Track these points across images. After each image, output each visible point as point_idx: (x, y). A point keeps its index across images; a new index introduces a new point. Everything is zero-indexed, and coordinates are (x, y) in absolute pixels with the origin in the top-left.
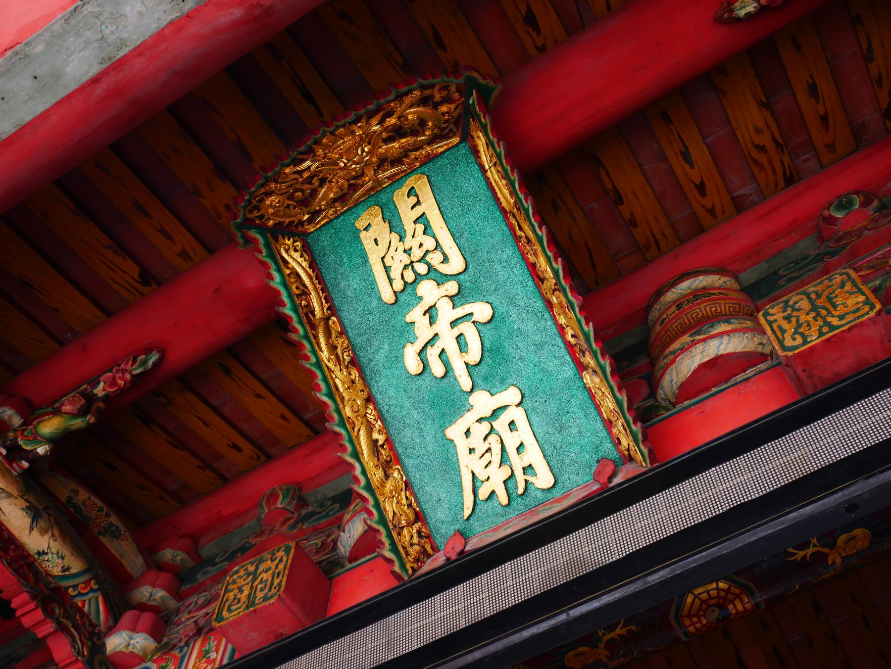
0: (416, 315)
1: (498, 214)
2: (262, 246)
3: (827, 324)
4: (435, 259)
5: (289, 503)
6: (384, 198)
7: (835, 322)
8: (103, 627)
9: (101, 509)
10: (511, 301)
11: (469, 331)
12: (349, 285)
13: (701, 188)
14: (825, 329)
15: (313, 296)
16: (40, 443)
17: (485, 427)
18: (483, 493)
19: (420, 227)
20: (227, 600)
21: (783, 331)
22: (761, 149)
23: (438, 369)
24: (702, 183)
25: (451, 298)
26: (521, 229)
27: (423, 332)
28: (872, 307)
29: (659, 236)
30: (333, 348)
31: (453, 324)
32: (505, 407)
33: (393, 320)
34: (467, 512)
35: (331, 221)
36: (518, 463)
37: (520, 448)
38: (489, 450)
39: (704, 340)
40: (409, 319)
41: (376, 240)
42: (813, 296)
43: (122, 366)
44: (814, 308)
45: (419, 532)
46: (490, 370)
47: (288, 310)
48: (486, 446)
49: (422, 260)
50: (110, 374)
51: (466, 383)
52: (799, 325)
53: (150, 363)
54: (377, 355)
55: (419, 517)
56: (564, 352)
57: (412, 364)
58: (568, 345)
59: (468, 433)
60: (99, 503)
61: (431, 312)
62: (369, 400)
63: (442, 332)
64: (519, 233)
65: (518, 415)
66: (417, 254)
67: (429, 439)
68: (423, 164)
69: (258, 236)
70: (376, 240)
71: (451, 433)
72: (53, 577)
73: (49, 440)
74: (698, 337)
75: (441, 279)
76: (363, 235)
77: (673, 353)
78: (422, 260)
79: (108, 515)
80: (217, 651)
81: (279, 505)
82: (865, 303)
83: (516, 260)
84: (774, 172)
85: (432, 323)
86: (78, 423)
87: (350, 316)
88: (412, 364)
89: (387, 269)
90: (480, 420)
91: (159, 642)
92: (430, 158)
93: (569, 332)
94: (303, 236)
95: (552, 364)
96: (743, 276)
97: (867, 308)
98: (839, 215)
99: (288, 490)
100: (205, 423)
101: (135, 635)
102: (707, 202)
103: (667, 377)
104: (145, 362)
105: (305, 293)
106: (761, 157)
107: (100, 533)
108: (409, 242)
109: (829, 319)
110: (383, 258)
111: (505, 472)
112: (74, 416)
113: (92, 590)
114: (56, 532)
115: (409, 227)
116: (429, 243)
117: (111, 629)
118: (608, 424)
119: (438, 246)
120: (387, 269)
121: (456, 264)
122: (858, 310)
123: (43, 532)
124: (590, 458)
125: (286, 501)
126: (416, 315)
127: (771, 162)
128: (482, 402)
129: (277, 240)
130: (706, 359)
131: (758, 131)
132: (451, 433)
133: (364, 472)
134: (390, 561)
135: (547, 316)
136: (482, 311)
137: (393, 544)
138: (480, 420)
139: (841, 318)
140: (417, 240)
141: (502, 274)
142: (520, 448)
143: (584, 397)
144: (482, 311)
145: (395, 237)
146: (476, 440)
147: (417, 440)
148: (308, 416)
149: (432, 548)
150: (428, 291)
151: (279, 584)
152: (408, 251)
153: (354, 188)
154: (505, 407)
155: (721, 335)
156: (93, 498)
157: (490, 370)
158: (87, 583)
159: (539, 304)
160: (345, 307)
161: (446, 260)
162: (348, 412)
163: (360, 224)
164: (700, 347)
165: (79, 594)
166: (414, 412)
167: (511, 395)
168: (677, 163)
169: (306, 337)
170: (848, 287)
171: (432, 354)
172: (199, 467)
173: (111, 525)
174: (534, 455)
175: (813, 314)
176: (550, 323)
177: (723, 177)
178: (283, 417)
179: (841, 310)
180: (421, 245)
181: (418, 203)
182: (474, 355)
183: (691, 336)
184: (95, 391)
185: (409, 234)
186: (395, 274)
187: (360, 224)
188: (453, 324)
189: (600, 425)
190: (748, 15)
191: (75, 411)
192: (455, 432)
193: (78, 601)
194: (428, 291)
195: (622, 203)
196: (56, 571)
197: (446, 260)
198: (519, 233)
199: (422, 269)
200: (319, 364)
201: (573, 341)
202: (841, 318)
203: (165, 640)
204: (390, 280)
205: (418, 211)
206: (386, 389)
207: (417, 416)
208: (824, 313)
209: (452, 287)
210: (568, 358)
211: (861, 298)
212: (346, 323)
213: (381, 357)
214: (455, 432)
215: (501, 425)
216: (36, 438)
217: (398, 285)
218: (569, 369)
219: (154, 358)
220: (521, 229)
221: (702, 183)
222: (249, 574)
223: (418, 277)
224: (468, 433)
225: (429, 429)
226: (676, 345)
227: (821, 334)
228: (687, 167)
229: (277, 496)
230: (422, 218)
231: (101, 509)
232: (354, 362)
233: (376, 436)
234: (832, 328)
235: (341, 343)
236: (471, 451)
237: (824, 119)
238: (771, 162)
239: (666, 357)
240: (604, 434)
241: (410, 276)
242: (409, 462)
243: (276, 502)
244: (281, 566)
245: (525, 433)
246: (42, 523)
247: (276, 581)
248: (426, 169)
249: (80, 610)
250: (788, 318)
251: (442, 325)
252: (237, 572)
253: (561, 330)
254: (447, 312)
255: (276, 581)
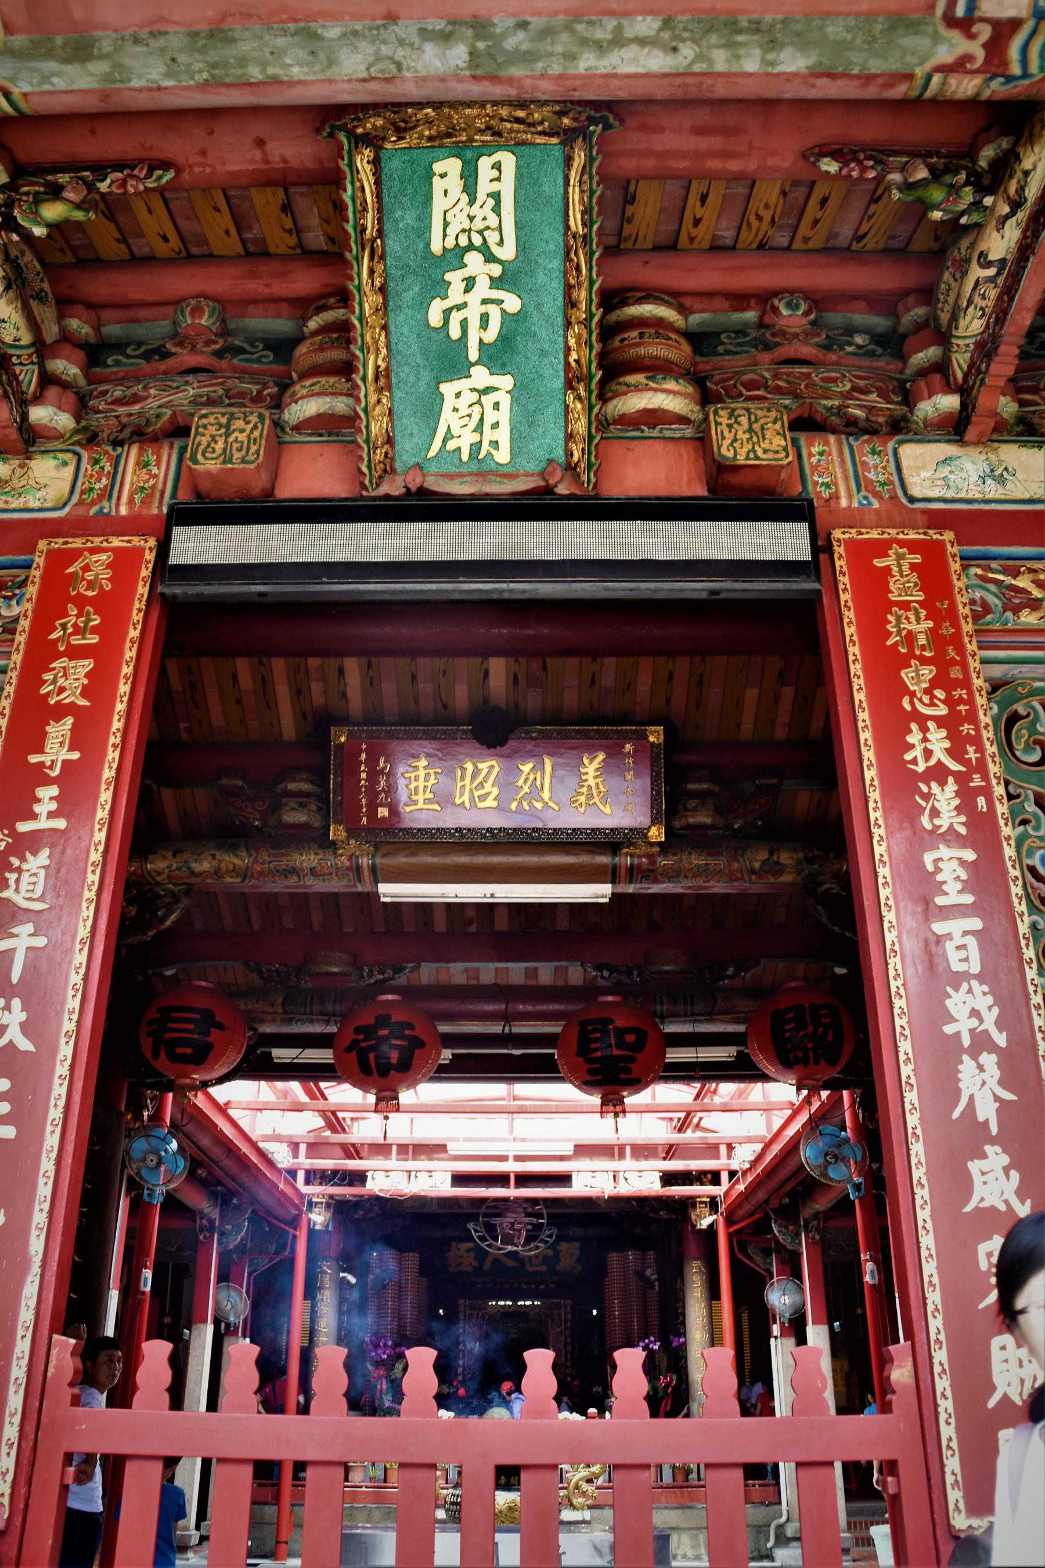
0: (455, 278)
1: (561, 227)
2: (345, 153)
3: (755, 452)
4: (492, 237)
5: (214, 323)
6: (469, 154)
7: (760, 453)
8: (29, 397)
9: (38, 274)
10: (538, 306)
11: (494, 311)
12: (405, 217)
13: (697, 222)
14: (751, 455)
15: (370, 216)
16: (39, 224)
17: (475, 396)
18: (451, 445)
19: (491, 202)
20: (199, 444)
21: (723, 438)
22: (760, 218)
23: (455, 332)
24: (700, 219)
25: (491, 278)
26: (576, 253)
27: (456, 294)
28: (787, 456)
29: (641, 236)
30: (372, 272)
31: (484, 302)
32: (497, 389)
33: (434, 271)
34: (431, 454)
35: (410, 148)
36: (488, 435)
37: (495, 426)
38: (470, 416)
39: (656, 390)
40: (448, 277)
41: (446, 192)
42: (753, 417)
43: (136, 172)
44: (750, 430)
45: (386, 454)
46: (496, 355)
47: (349, 228)
48: (469, 411)
49: (481, 232)
50: (120, 175)
51: (473, 355)
52: (735, 440)
53: (164, 180)
54: (408, 292)
55: (390, 441)
56: (561, 367)
57: (435, 318)
58: (567, 364)
59: (458, 395)
60: (38, 267)
61: (470, 283)
62: (384, 327)
63: (472, 305)
64: (573, 256)
65: (505, 400)
66: (478, 224)
67: (423, 383)
68: (517, 144)
69: (345, 141)
70: (446, 192)
71: (444, 388)
72: (4, 343)
73: (49, 225)
74: (654, 385)
75: (490, 258)
76: (436, 180)
77: (627, 385)
78: (481, 232)
79: (42, 281)
80: (158, 465)
81: (203, 322)
82: (785, 449)
83: (559, 275)
84: (756, 236)
85: (467, 290)
86: (79, 215)
87: (393, 244)
88: (435, 318)
89: (446, 224)
90: (472, 390)
91: (78, 422)
92: (524, 143)
93: (574, 356)
94: (378, 149)
95: (548, 373)
96: (695, 319)
97: (783, 454)
98: (785, 312)
99: (214, 309)
100: (150, 211)
101: (60, 413)
102: (694, 232)
103: (614, 402)
104: (160, 178)
105: (365, 210)
106: (755, 223)
107: (31, 296)
108: (475, 210)
109: (757, 448)
110: (445, 212)
111: (476, 438)
112: (78, 206)
113: (32, 363)
114: (19, 304)
115: (481, 196)
116: (493, 221)
117: (38, 399)
118: (569, 437)
119: (500, 229)
120: (446, 224)
121: (508, 252)
122: (777, 452)
123: (10, 302)
124: (543, 454)
125: (212, 320)
126: (455, 278)
127: (759, 229)
128: (480, 376)
129: (357, 147)
130: (650, 406)
131: (767, 206)
132: (444, 388)
133: (366, 396)
134: (364, 474)
135: (561, 332)
136: (513, 303)
137: (369, 461)
138: (472, 390)
139: (765, 451)
140: (483, 211)
141: (541, 279)
142: (495, 426)
143: (561, 409)
144: (513, 303)
145: (465, 198)
146: (463, 404)
147: (412, 379)
148: (247, 235)
149: (392, 468)
150: (474, 261)
151: (258, 452)
152: (471, 219)
153: (449, 135)
154: (497, 389)
155: (669, 392)
156: (35, 262)
157: (496, 355)
158: (30, 356)
159: (560, 320)
160: (392, 236)
161: (501, 242)
162: (368, 338)
163: (438, 167)
164: (650, 394)
165: (21, 364)
166: (418, 355)
167: (506, 382)
168: (693, 199)
169: (357, 259)
170: (778, 426)
171: (456, 318)
172: (118, 240)
173: (42, 290)
174: (503, 436)
175: (747, 436)
176: (561, 339)
177: (718, 218)
178: (227, 232)
179: (765, 445)
180: (485, 219)
181: (498, 179)
182: (491, 335)
183: (647, 378)
184: (99, 185)
185: (479, 202)
186: (452, 231)
187: (438, 167)
188: (484, 302)
189: (562, 435)
190: (827, 172)
191: (78, 201)
192: (447, 389)
193: (17, 369)
194: (474, 261)
195: (632, 204)
196: (8, 339)
197: (501, 242)
198: (573, 256)
199: (477, 240)
200: (359, 288)
201: (573, 364)
202: (765, 451)
203: (84, 423)
204: (445, 235)
205: (495, 187)
206: (402, 321)
207: (420, 360)
208: (755, 439)
209: (496, 270)
210: (562, 374)
211: (783, 443)
212: (388, 250)
213: (408, 296)
214: (447, 389)
215: (488, 400)
216: (36, 216)
217: (450, 243)
218: (559, 383)
219: (170, 175)
220: (576, 253)
221: (700, 219)
222: (221, 426)
223: (471, 247)
224: (458, 395)
225: (426, 375)
226: (632, 379)
227: (747, 458)
228: (699, 204)
229: (202, 312)
230: (496, 196)
231: (38, 274)
232: (382, 290)
233: (380, 362)
234: (757, 458)
235: (379, 268)
236: (455, 410)
237: (816, 221)
238: (759, 229)
239: (619, 384)
240: (562, 442)
241: (463, 241)
242: (398, 394)
243: (201, 318)
244: (256, 434)
245: (504, 416)
246: (11, 294)
247: (254, 448)
248: (517, 150)
249: (16, 377)
250: (730, 426)
251: (474, 298)
252: (205, 416)
253: (568, 350)
254: (482, 289)
255: (254, 448)
